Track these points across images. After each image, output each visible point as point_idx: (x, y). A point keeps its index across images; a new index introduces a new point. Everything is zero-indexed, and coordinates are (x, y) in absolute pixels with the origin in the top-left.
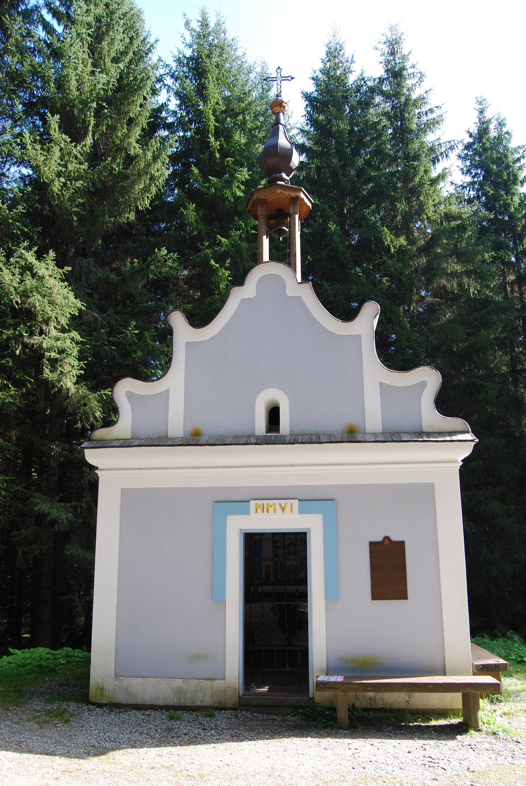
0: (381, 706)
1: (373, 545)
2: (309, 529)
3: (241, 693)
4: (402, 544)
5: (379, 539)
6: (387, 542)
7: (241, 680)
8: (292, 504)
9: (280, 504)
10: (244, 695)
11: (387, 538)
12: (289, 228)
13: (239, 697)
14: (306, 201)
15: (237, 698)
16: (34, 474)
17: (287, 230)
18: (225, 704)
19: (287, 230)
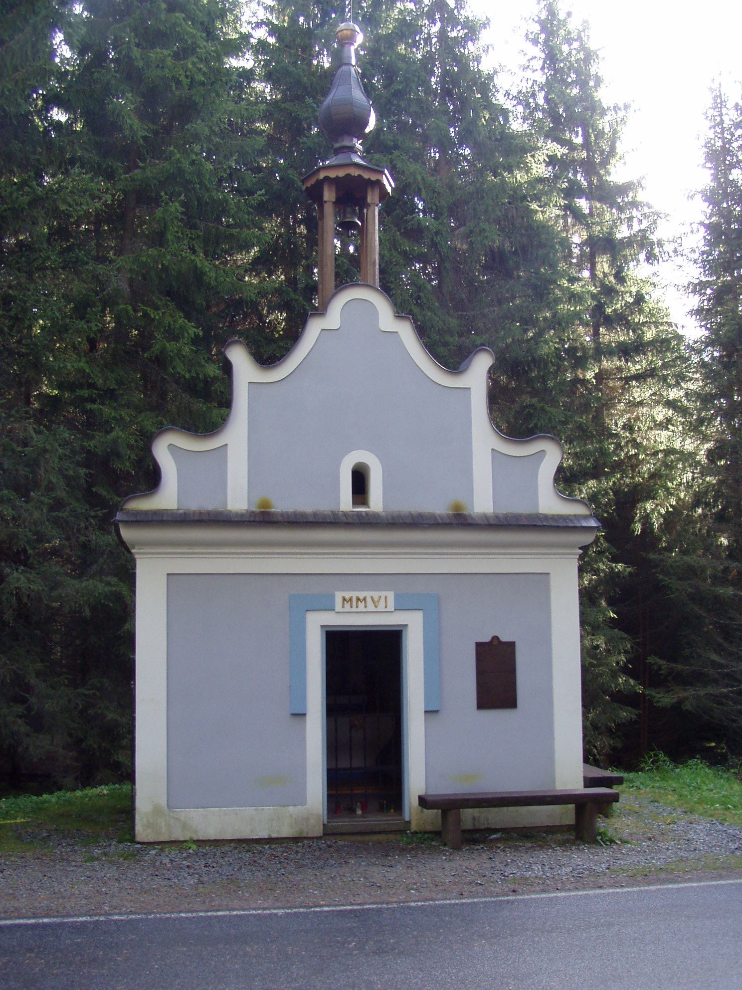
0: (486, 826)
1: (479, 645)
2: (406, 626)
3: (325, 822)
4: (512, 645)
5: (487, 639)
6: (495, 643)
7: (326, 812)
8: (386, 598)
9: (372, 598)
10: (328, 822)
11: (495, 638)
12: (362, 221)
13: (324, 825)
14: (494, 836)
15: (322, 827)
16: (578, 308)
17: (360, 224)
18: (308, 833)
19: (360, 224)
